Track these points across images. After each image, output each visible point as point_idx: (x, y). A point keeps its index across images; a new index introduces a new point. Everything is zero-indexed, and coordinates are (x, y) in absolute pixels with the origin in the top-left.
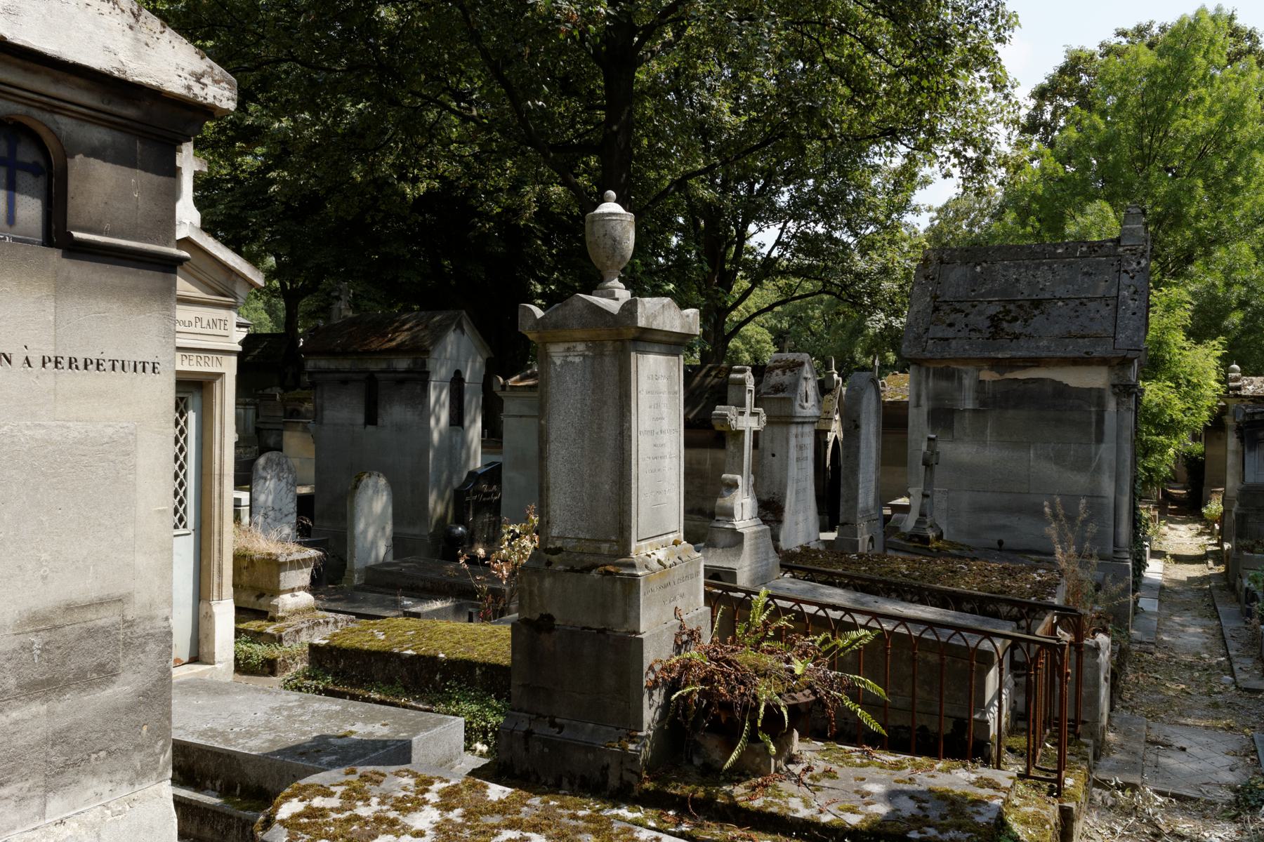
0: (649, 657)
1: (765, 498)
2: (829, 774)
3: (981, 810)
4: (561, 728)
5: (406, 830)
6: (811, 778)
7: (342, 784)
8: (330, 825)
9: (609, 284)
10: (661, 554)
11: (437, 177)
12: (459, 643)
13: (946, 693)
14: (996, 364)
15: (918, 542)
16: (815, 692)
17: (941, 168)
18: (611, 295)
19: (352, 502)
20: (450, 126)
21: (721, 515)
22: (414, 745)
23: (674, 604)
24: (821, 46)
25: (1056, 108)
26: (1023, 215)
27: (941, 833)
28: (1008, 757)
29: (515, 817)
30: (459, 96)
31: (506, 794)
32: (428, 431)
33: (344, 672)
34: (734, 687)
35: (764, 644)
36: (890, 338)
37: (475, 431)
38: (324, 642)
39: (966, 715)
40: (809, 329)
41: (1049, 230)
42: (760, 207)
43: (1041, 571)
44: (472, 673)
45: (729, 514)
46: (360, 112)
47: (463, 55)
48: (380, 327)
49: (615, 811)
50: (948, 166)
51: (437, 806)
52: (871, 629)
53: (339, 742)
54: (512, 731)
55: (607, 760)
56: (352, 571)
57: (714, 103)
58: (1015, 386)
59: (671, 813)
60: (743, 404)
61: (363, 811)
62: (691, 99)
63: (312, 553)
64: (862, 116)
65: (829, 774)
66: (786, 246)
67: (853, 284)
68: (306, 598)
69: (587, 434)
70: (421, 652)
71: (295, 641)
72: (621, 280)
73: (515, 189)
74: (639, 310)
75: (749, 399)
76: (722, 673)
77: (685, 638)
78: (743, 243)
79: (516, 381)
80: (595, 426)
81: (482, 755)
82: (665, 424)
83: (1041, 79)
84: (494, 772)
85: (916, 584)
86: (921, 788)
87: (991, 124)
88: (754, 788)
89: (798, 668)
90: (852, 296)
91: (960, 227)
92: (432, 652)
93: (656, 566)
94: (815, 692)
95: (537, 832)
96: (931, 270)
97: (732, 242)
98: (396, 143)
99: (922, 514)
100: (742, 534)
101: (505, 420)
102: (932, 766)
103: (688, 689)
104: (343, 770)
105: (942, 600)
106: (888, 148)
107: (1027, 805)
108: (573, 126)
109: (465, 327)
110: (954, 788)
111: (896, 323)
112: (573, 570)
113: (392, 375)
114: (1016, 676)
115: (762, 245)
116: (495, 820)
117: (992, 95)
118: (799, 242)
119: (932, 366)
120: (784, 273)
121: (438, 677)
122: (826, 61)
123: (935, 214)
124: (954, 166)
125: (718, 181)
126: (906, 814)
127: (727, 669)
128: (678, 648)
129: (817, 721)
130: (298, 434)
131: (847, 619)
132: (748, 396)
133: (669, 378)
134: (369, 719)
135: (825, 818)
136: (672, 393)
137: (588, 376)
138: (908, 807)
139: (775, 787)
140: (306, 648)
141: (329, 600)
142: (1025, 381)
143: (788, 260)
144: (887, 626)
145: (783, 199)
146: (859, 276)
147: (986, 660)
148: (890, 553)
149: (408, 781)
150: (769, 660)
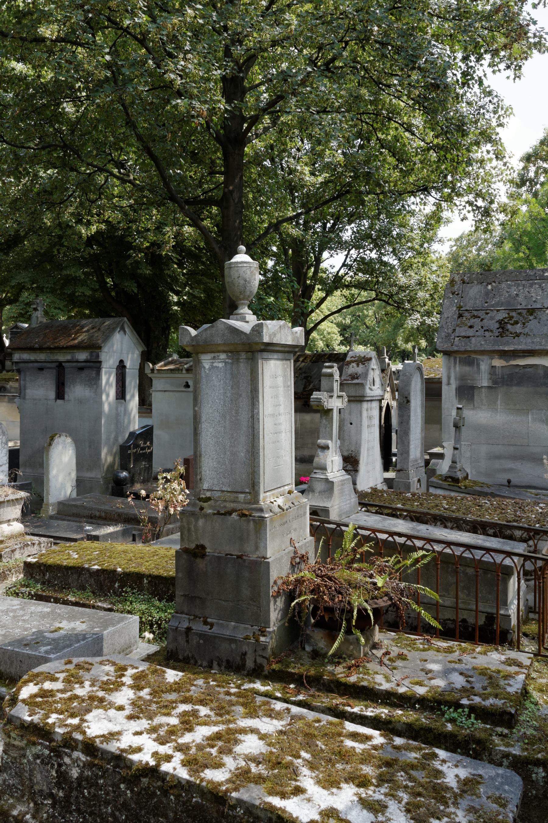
1: (346, 454)
2: (402, 657)
3: (511, 682)
4: (212, 625)
5: (111, 705)
6: (389, 660)
7: (63, 672)
8: (58, 702)
9: (241, 311)
10: (280, 501)
11: (104, 221)
12: (131, 560)
13: (480, 595)
14: (503, 354)
15: (452, 481)
16: (391, 599)
17: (460, 213)
18: (243, 319)
19: (48, 455)
20: (113, 186)
21: (317, 469)
22: (105, 637)
23: (289, 536)
24: (375, 130)
25: (539, 168)
26: (517, 244)
27: (484, 700)
28: (524, 641)
29: (188, 695)
30: (121, 165)
31: (179, 677)
32: (101, 404)
33: (49, 581)
36: (426, 331)
37: (134, 402)
38: (34, 560)
39: (494, 611)
40: (365, 324)
41: (535, 255)
42: (331, 240)
43: (541, 505)
44: (141, 582)
45: (324, 469)
46: (51, 177)
47: (125, 139)
48: (64, 330)
49: (252, 685)
50: (465, 212)
51: (131, 687)
52: (427, 551)
53: (52, 635)
54: (177, 628)
55: (245, 648)
56: (48, 505)
57: (299, 168)
58: (517, 370)
59: (292, 686)
60: (332, 390)
61: (80, 691)
62: (281, 164)
63: (23, 494)
64: (404, 177)
65: (402, 657)
66: (350, 267)
67: (397, 293)
68: (18, 527)
69: (228, 417)
70: (104, 567)
71: (11, 558)
72: (249, 307)
73: (159, 228)
74: (264, 331)
75: (336, 386)
76: (326, 586)
77: (298, 560)
80: (233, 412)
81: (149, 641)
82: (282, 409)
83: (527, 147)
84: (168, 658)
85: (454, 515)
86: (467, 667)
87: (495, 183)
88: (349, 668)
90: (397, 302)
91: (471, 252)
92: (112, 567)
93: (277, 510)
94: (391, 599)
95: (203, 705)
96: (456, 288)
98: (75, 198)
99: (454, 462)
100: (333, 482)
101: (153, 394)
102: (474, 650)
103: (302, 598)
104: (63, 661)
105: (476, 527)
106: (422, 199)
107: (541, 677)
109: (127, 330)
110: (490, 666)
111: (428, 321)
112: (219, 513)
113: (74, 364)
114: (527, 580)
115: (332, 267)
116: (173, 696)
117: (495, 163)
119: (458, 356)
120: (348, 287)
122: (378, 139)
123: (453, 243)
124: (469, 212)
126: (458, 686)
127: (329, 583)
128: (293, 566)
129: (395, 619)
130: (5, 404)
131: (409, 543)
132: (335, 384)
133: (285, 376)
134: (71, 618)
135: (402, 690)
136: (286, 386)
137: (228, 376)
138: (459, 681)
139: (364, 667)
140: (22, 565)
141: (36, 527)
142: (525, 367)
143: (351, 277)
144: (438, 548)
145: (347, 235)
146: (402, 288)
147: (507, 572)
148: (432, 490)
149: (109, 668)
150: (358, 576)
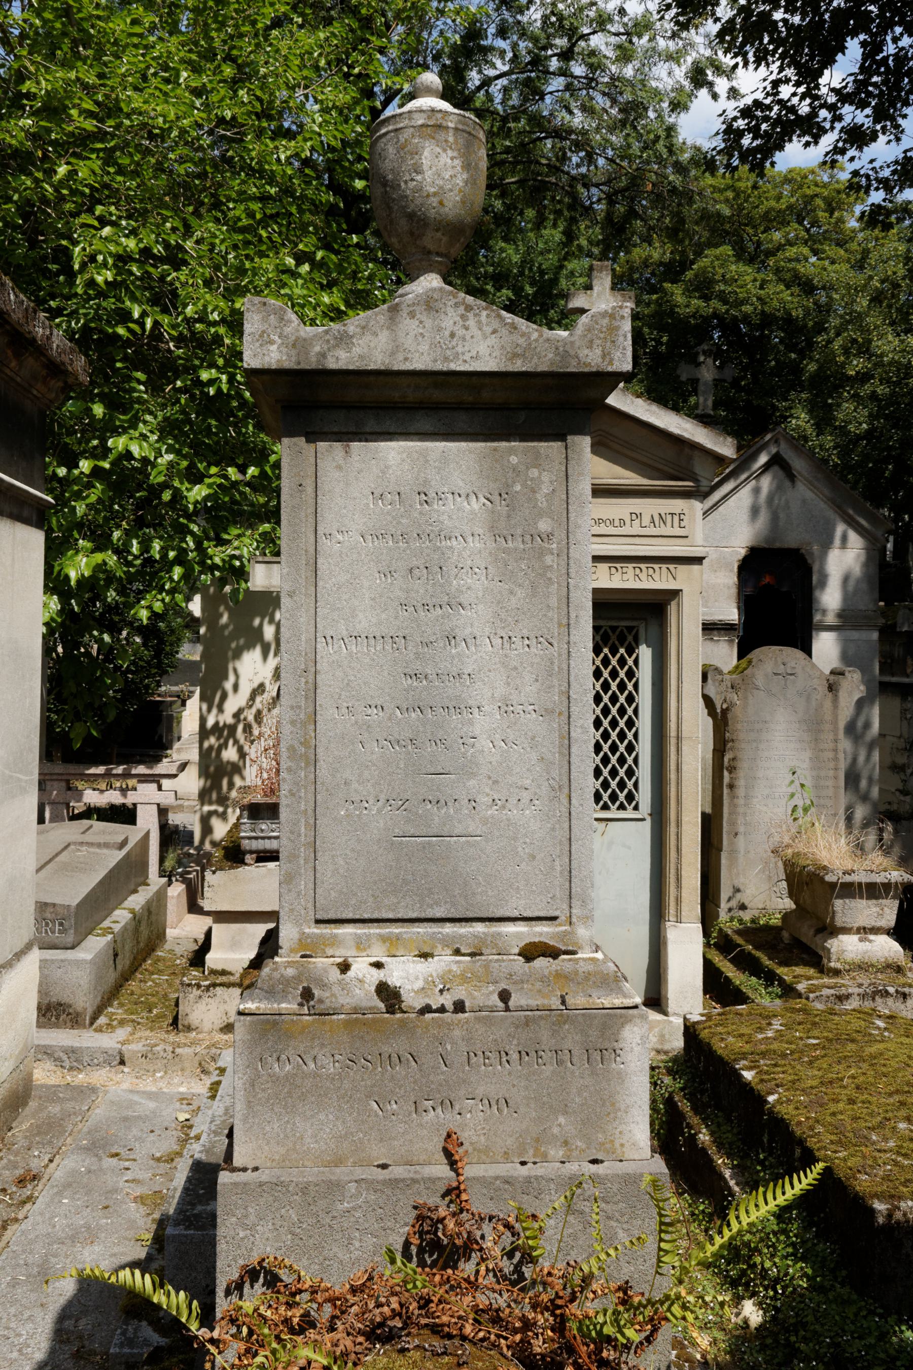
68: (887, 947)
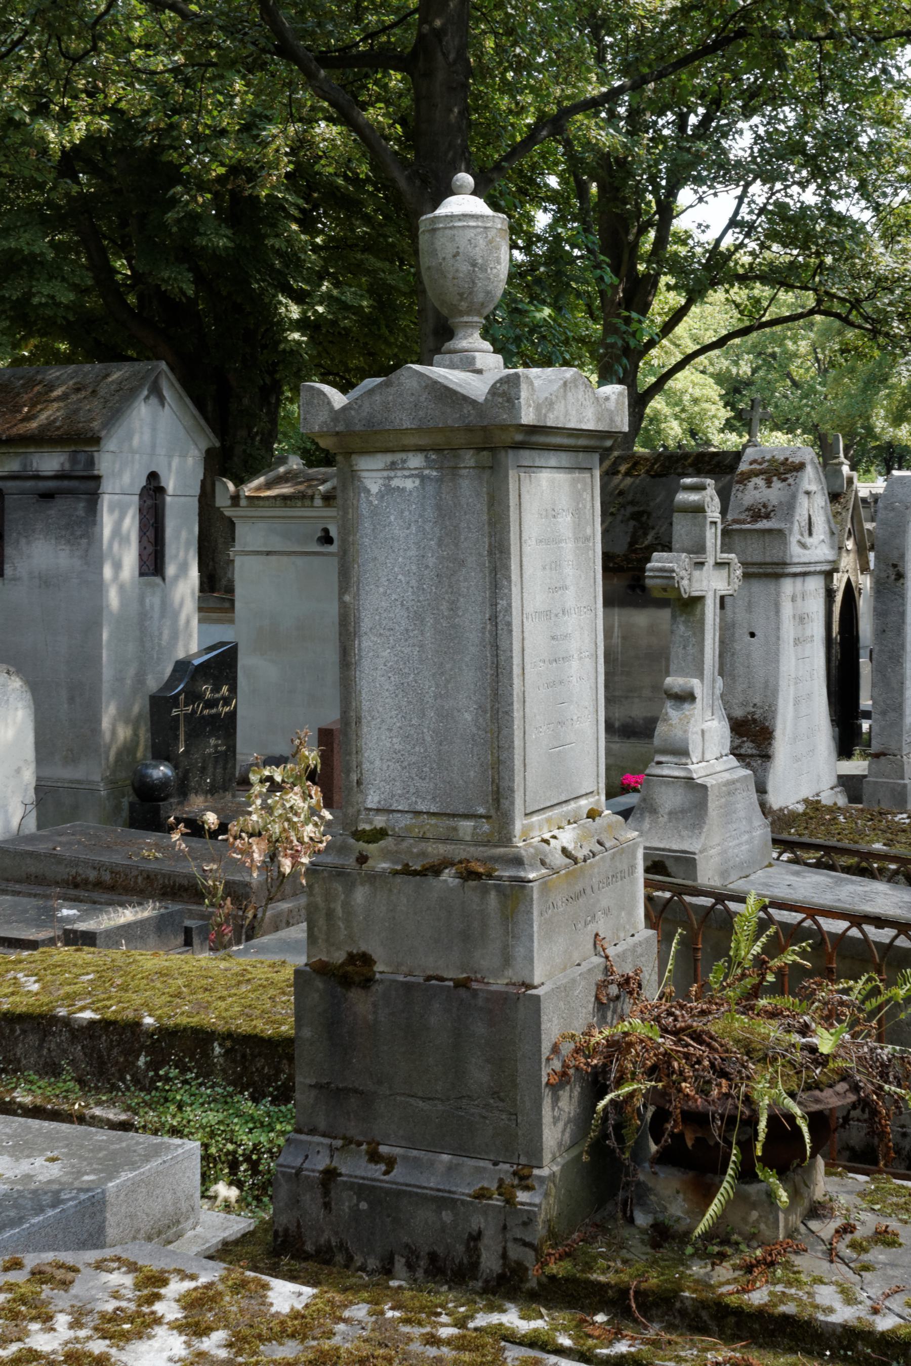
0: (552, 1028)
1: (739, 713)
4: (390, 1163)
6: (853, 1245)
9: (464, 344)
10: (567, 837)
11: (106, 110)
12: (178, 995)
18: (469, 365)
21: (665, 752)
22: (111, 1197)
23: (592, 928)
29: (326, 1345)
31: (304, 1300)
32: (99, 587)
34: (709, 1082)
35: (763, 1002)
37: (185, 582)
40: (789, 375)
42: (699, 158)
44: (207, 1054)
49: (495, 1318)
54: (299, 1170)
59: (600, 1318)
60: (700, 549)
66: (749, 229)
67: (872, 296)
70: (109, 1015)
72: (486, 334)
73: (250, 128)
74: (524, 394)
75: (712, 538)
76: (687, 1056)
77: (614, 990)
78: (669, 223)
79: (258, 489)
80: (444, 606)
82: (570, 598)
89: (825, 1042)
92: (130, 1014)
93: (559, 860)
94: (855, 1088)
97: (649, 223)
98: (30, 49)
100: (704, 787)
101: (238, 561)
103: (626, 1089)
108: (358, 20)
109: (166, 393)
112: (407, 871)
113: (29, 484)
115: (703, 227)
118: (770, 221)
120: (744, 279)
121: (142, 1061)
125: (622, 110)
127: (696, 1049)
128: (604, 1006)
133: (577, 513)
135: (884, 1324)
136: (582, 539)
137: (430, 513)
139: (788, 1265)
143: (752, 253)
145: (741, 145)
149: (121, 1279)
150: (771, 1030)
